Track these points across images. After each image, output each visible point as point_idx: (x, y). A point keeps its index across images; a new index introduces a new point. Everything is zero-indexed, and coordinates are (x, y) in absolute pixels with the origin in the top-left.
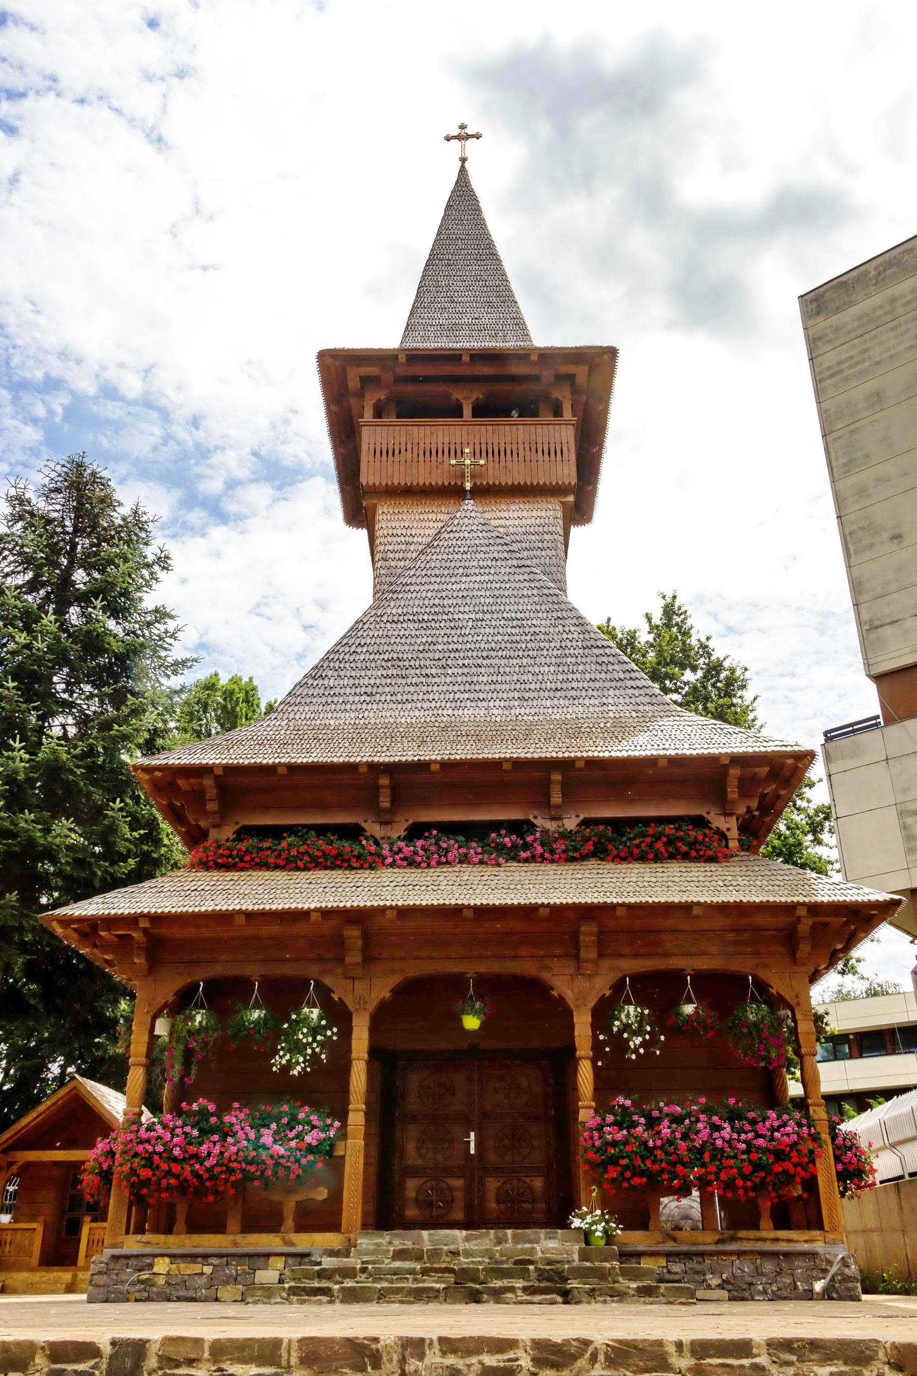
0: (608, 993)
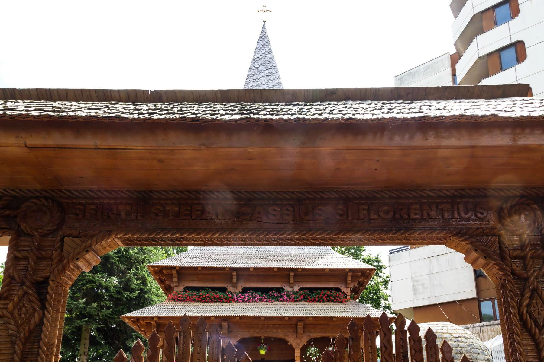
0: (306, 344)
